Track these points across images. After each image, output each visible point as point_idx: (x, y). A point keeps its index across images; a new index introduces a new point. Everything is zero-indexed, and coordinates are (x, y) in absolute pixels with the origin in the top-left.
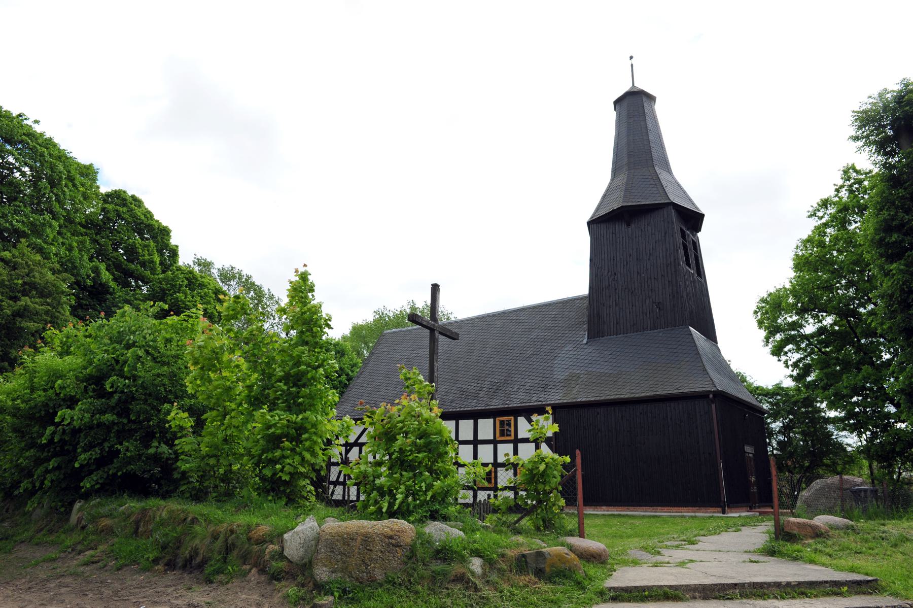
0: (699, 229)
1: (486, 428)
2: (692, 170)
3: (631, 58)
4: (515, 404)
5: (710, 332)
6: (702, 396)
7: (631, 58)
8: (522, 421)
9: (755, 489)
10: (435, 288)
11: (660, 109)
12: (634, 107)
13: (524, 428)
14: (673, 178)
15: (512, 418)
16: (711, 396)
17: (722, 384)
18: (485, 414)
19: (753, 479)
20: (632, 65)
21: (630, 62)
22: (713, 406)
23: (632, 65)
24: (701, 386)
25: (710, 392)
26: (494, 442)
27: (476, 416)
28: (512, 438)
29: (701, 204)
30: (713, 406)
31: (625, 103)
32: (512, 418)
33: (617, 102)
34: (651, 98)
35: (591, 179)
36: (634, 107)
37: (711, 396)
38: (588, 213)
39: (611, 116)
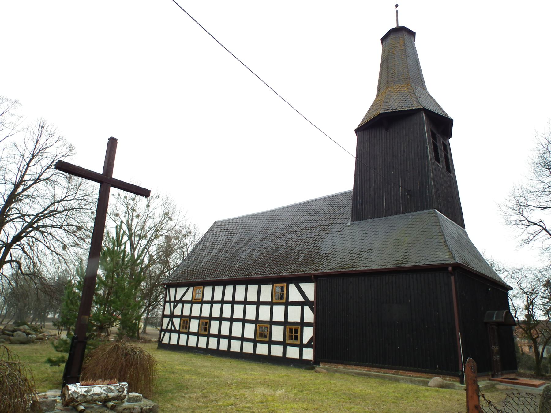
0: (450, 136)
1: (266, 292)
2: (442, 88)
3: (397, 6)
4: (286, 274)
5: (457, 216)
6: (441, 269)
7: (397, 6)
8: (292, 288)
9: (498, 358)
10: (112, 143)
11: (419, 44)
12: (399, 41)
13: (294, 295)
14: (427, 92)
15: (285, 284)
16: (450, 268)
17: (426, 104)
18: (265, 281)
19: (495, 349)
20: (397, 12)
21: (396, 10)
22: (452, 278)
23: (397, 12)
24: (439, 257)
25: (449, 265)
26: (271, 304)
27: (259, 282)
28: (284, 301)
29: (449, 109)
30: (452, 278)
31: (389, 40)
32: (285, 284)
33: (383, 39)
34: (412, 34)
35: (361, 97)
36: (399, 41)
37: (450, 268)
38: (357, 121)
39: (378, 49)
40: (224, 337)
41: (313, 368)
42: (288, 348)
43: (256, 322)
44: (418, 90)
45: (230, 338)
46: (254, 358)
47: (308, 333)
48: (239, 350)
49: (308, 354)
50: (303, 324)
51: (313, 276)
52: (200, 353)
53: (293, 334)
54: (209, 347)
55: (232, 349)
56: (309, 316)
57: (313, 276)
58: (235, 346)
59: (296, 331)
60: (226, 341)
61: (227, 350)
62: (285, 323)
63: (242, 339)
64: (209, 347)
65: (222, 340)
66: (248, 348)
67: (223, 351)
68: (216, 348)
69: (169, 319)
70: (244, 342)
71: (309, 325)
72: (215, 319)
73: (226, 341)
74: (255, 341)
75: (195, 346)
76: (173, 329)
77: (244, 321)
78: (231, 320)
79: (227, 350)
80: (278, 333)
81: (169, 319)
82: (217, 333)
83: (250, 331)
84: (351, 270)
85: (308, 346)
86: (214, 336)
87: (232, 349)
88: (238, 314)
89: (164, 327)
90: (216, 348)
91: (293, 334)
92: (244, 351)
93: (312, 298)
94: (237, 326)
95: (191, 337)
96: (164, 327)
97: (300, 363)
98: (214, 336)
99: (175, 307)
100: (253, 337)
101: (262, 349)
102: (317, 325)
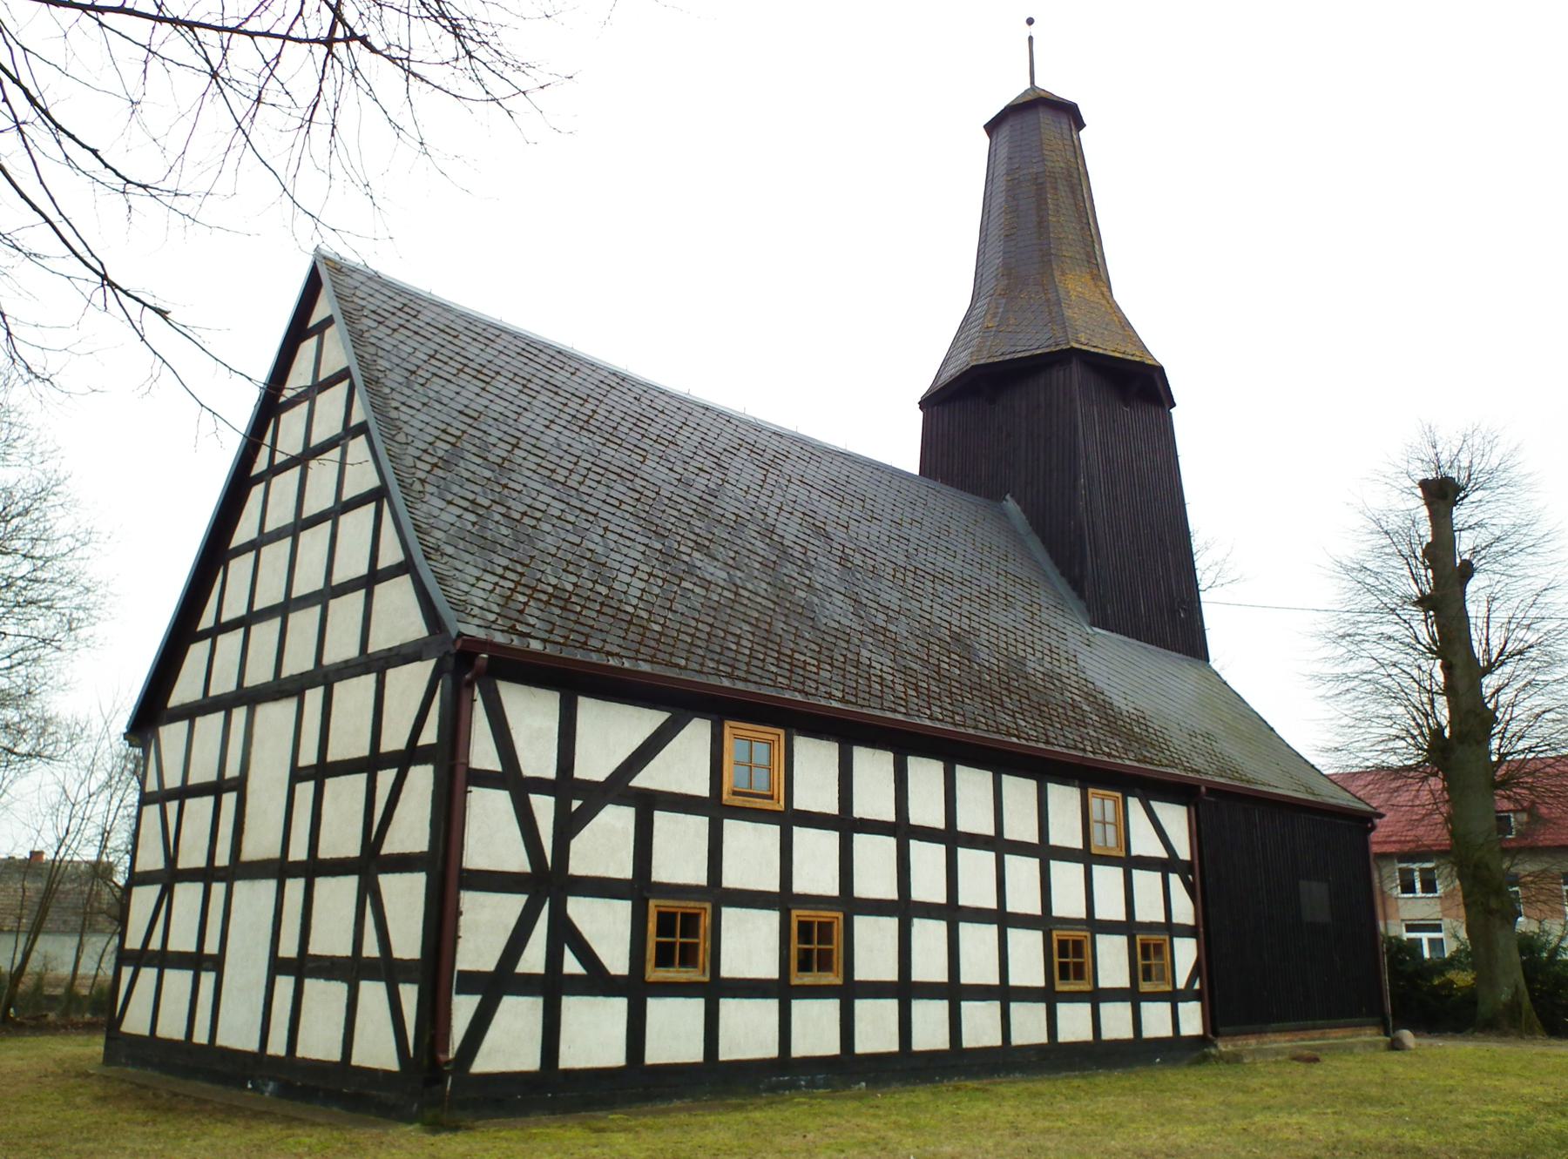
34: (1069, 114)
40: (930, 991)
41: (1205, 1059)
42: (1144, 1006)
43: (1044, 921)
44: (1074, 285)
45: (954, 992)
46: (1055, 1058)
47: (1186, 953)
48: (146, 1032)
49: (1192, 1019)
50: (1171, 929)
51: (1203, 789)
52: (812, 1085)
53: (679, 940)
54: (860, 1048)
55: (968, 1041)
56: (1184, 911)
57: (1203, 789)
58: (981, 1025)
59: (691, 921)
60: (941, 1008)
61: (895, 1048)
62: (783, 900)
63: (1004, 993)
64: (860, 1048)
65: (919, 1008)
66: (1029, 1025)
67: (932, 1056)
68: (894, 1047)
69: (515, 903)
70: (1013, 1006)
71: (1185, 931)
72: (877, 907)
73: (941, 1008)
74: (1048, 996)
75: (773, 1052)
76: (572, 965)
77: (1002, 919)
78: (952, 913)
79: (895, 1048)
80: (749, 943)
81: (515, 903)
82: (890, 974)
83: (1028, 961)
84: (1170, 770)
85: (1187, 995)
86: (877, 990)
87: (968, 1041)
88: (977, 889)
89: (134, 941)
90: (894, 1047)
91: (815, 946)
92: (1064, 1036)
93: (1184, 853)
94: (978, 942)
95: (1106, 1009)
96: (134, 941)
97: (1175, 1049)
98: (877, 990)
99: (567, 826)
100: (773, 973)
101: (1074, 1023)
102: (1202, 931)
